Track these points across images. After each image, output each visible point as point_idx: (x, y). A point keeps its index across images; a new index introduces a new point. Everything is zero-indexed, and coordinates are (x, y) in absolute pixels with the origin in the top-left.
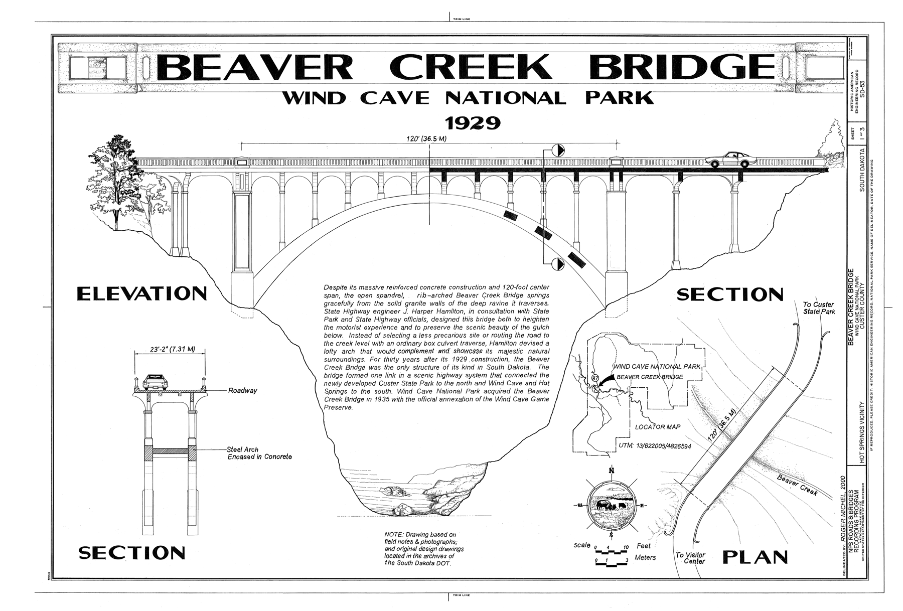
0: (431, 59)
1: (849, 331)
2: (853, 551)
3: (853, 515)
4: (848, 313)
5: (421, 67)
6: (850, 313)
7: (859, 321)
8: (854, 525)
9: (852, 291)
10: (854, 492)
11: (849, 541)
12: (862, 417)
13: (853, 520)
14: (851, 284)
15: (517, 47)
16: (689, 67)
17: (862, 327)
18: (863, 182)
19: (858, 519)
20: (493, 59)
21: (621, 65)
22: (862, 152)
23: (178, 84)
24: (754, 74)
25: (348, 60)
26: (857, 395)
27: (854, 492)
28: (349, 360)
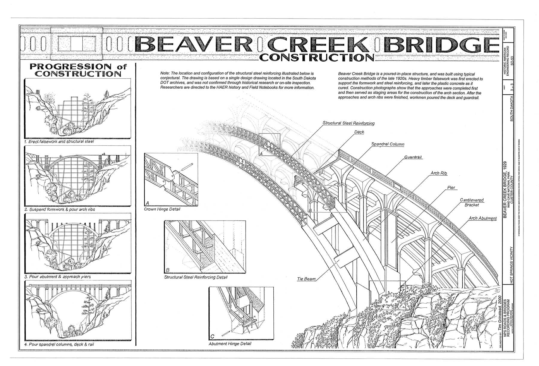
0: (293, 40)
1: (503, 209)
2: (506, 336)
3: (506, 314)
4: (503, 199)
5: (286, 45)
6: (505, 199)
7: (510, 199)
8: (507, 320)
9: (505, 186)
10: (507, 301)
11: (503, 330)
12: (512, 256)
13: (506, 317)
14: (505, 182)
15: (347, 34)
16: (446, 45)
17: (512, 202)
18: (512, 116)
19: (510, 316)
20: (331, 40)
21: (404, 44)
22: (512, 98)
23: (146, 55)
24: (487, 50)
25: (250, 41)
26: (508, 244)
27: (507, 301)
28: (49, 345)
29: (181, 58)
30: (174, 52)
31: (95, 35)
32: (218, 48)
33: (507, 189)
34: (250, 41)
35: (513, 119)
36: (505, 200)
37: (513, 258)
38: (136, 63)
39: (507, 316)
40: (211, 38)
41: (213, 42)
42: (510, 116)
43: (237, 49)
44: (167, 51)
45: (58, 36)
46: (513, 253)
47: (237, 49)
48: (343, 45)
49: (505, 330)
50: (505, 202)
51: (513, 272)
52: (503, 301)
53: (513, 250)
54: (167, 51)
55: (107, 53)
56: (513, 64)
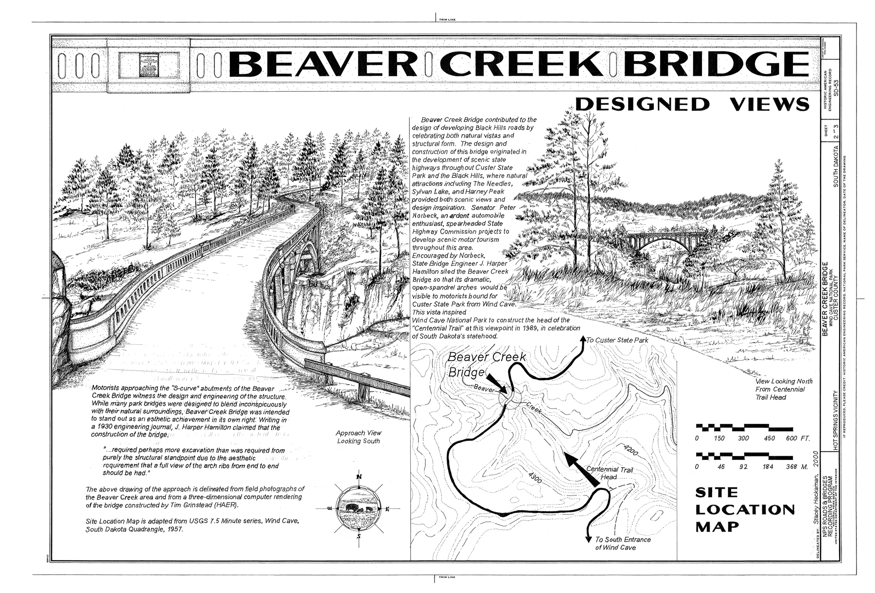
0: (480, 55)
3: (827, 500)
8: (828, 510)
10: (828, 478)
11: (822, 526)
12: (836, 405)
16: (725, 63)
17: (836, 318)
20: (543, 56)
22: (836, 149)
24: (789, 72)
25: (413, 57)
27: (828, 478)
29: (347, 87)
30: (294, 78)
31: (177, 50)
32: (362, 71)
33: (828, 289)
34: (413, 57)
35: (839, 183)
36: (825, 306)
37: (838, 410)
38: (807, 64)
39: (828, 504)
40: (351, 53)
41: (354, 61)
42: (833, 178)
43: (393, 72)
44: (126, 78)
45: (120, 53)
46: (838, 400)
47: (393, 72)
48: (381, 64)
49: (825, 525)
50: (825, 310)
51: (837, 432)
52: (822, 479)
53: (838, 396)
54: (126, 78)
55: (59, 80)
56: (839, 93)
